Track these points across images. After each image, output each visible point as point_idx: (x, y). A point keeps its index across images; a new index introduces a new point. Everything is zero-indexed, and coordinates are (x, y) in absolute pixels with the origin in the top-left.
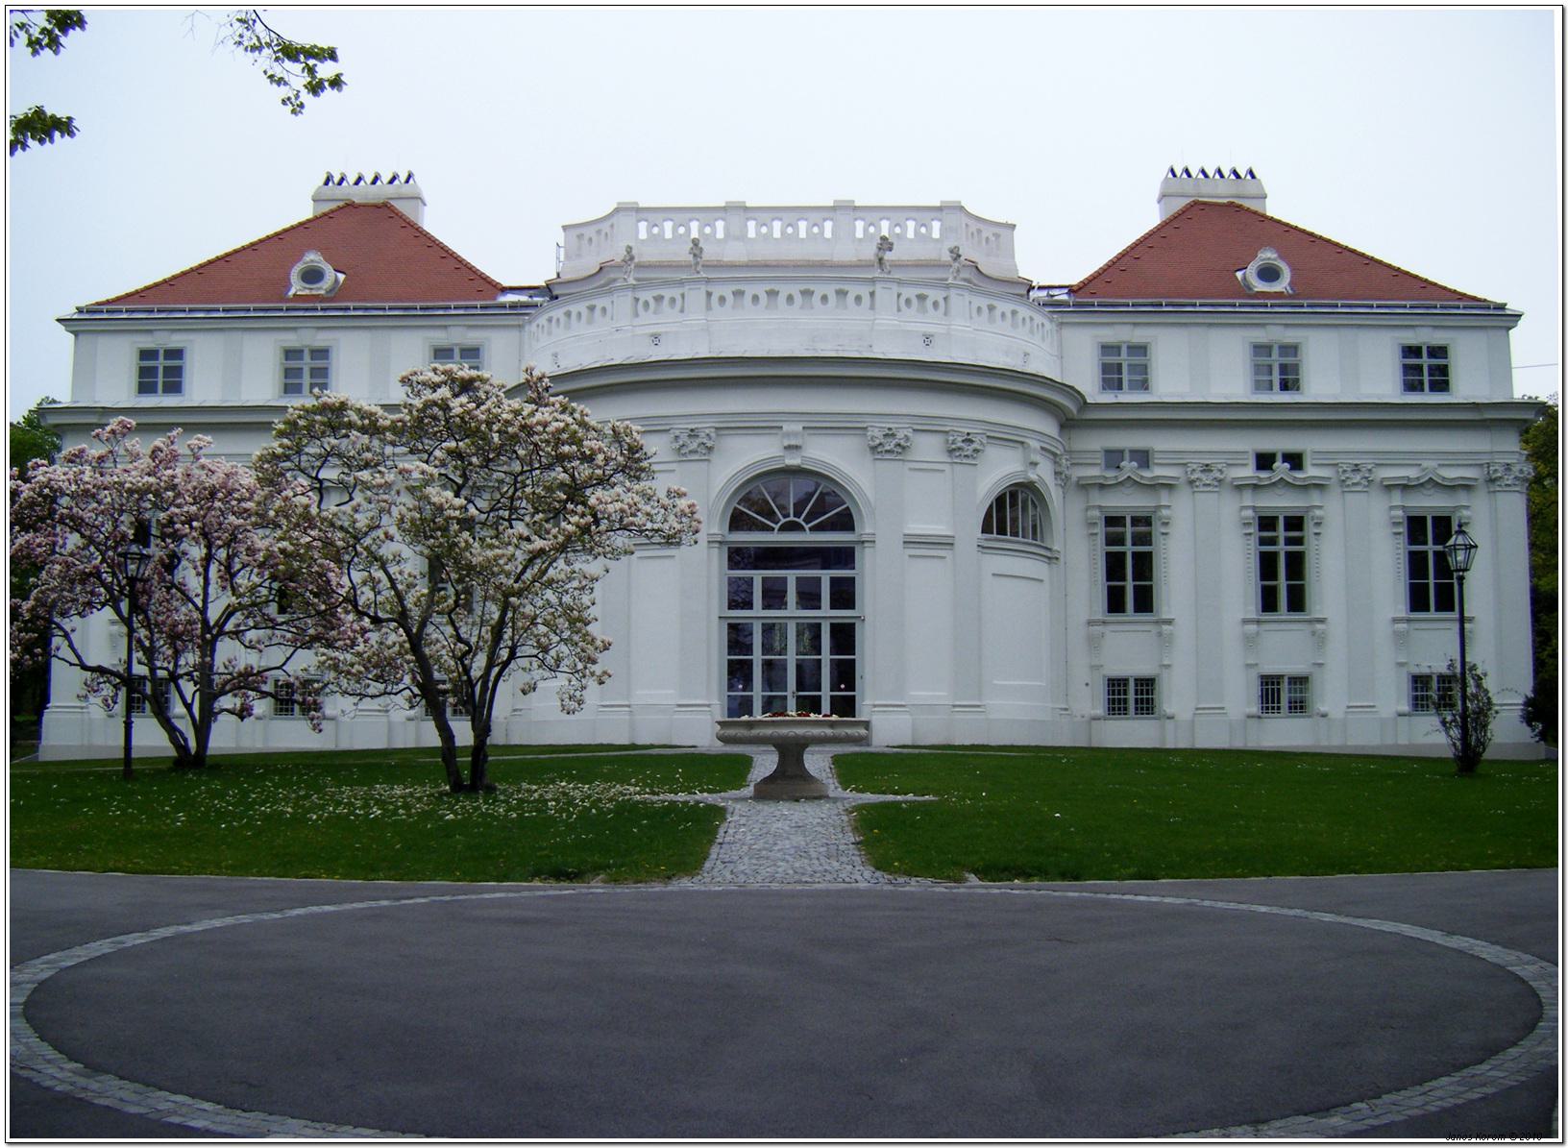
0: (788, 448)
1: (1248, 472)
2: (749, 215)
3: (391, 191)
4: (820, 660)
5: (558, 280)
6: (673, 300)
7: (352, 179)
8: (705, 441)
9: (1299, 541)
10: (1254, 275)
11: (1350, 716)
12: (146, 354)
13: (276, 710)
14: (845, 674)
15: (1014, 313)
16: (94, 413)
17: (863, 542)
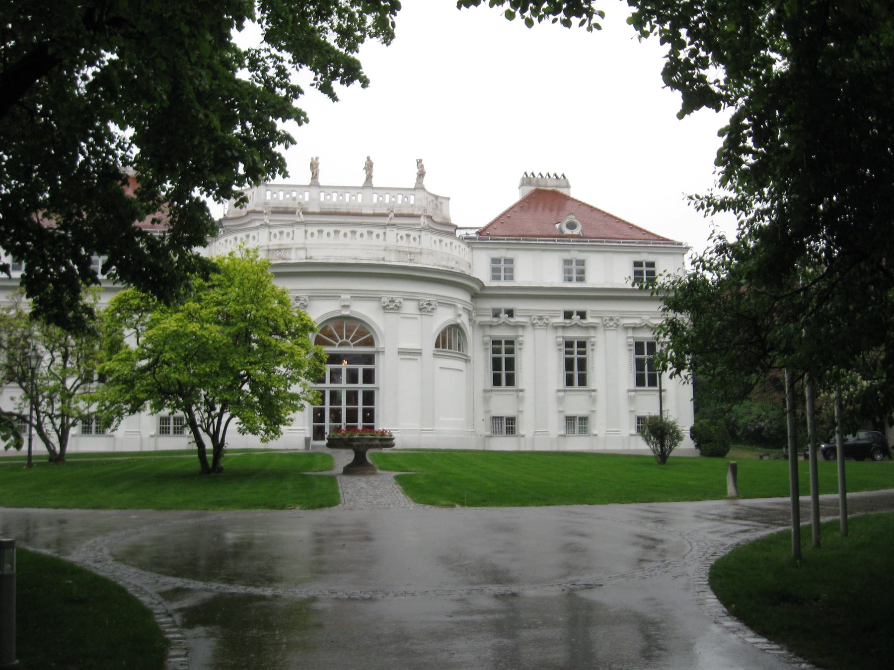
9: (584, 353)
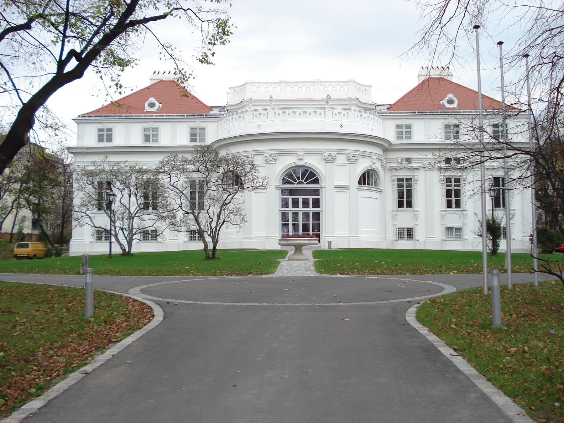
2: (287, 84)
4: (319, 223)
5: (228, 105)
8: (274, 157)
9: (459, 186)
11: (475, 240)
12: (101, 130)
14: (317, 227)
16: (85, 149)
17: (322, 188)
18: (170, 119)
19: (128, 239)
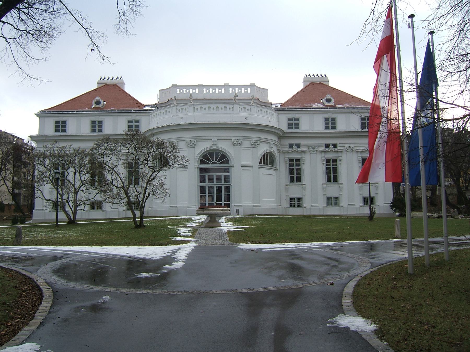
0: (213, 144)
1: (323, 148)
3: (117, 81)
6: (186, 109)
7: (107, 78)
9: (336, 165)
10: (325, 101)
13: (91, 209)
14: (228, 198)
15: (267, 111)
18: (112, 113)
19: (73, 209)
